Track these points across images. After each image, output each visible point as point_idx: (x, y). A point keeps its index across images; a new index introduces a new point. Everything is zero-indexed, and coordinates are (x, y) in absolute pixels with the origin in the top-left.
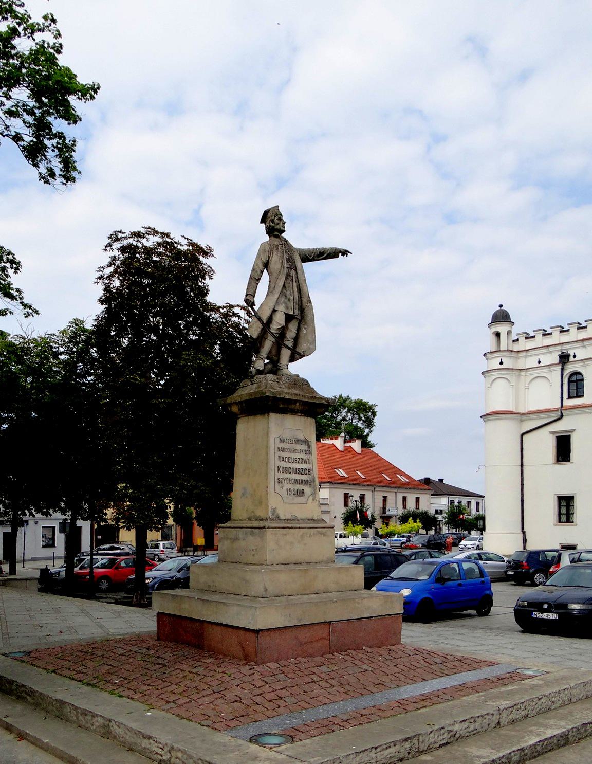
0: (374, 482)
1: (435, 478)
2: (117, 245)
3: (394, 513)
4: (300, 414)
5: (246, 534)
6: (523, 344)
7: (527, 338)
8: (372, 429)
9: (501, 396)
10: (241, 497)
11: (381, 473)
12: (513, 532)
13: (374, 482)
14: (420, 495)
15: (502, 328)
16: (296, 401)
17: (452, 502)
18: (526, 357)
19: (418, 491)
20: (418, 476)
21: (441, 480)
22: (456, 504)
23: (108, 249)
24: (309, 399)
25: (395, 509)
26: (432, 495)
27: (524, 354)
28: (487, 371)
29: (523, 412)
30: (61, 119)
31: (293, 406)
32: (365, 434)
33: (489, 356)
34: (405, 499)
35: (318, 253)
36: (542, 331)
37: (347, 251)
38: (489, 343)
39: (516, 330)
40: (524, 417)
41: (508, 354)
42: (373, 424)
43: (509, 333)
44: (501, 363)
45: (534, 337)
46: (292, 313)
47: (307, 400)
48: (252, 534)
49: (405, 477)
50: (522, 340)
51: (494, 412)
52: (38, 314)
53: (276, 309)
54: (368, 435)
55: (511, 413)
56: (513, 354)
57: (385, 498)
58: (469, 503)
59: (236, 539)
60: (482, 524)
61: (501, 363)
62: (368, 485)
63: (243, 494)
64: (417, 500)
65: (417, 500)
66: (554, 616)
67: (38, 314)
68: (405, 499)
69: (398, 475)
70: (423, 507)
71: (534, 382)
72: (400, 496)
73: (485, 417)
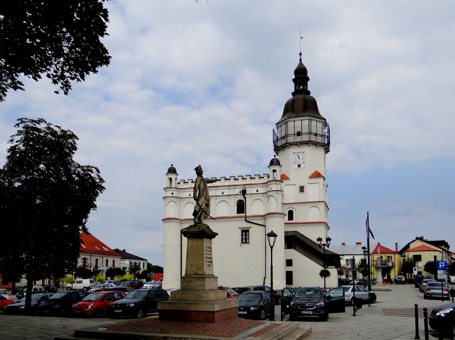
0: (91, 251)
1: (121, 249)
2: (22, 125)
3: (102, 269)
5: (195, 280)
6: (182, 186)
7: (184, 183)
8: (87, 220)
9: (172, 211)
10: (190, 267)
11: (94, 245)
12: (178, 279)
13: (91, 251)
14: (115, 258)
15: (173, 176)
17: (131, 263)
18: (184, 192)
19: (114, 257)
20: (113, 248)
21: (124, 251)
22: (133, 264)
23: (17, 126)
25: (103, 267)
26: (121, 259)
27: (183, 190)
28: (165, 197)
29: (182, 219)
32: (83, 222)
33: (166, 189)
34: (107, 261)
36: (191, 180)
38: (166, 184)
39: (179, 178)
40: (183, 222)
41: (175, 189)
42: (88, 217)
43: (176, 179)
44: (172, 194)
45: (188, 182)
48: (199, 280)
49: (107, 248)
50: (182, 183)
51: (169, 218)
54: (85, 223)
55: (177, 219)
56: (178, 190)
57: (97, 260)
58: (140, 263)
59: (191, 282)
60: (149, 275)
61: (172, 194)
62: (88, 253)
63: (191, 266)
64: (114, 261)
65: (114, 261)
66: (245, 313)
68: (107, 261)
69: (103, 247)
70: (117, 265)
71: (187, 205)
72: (105, 259)
73: (164, 220)
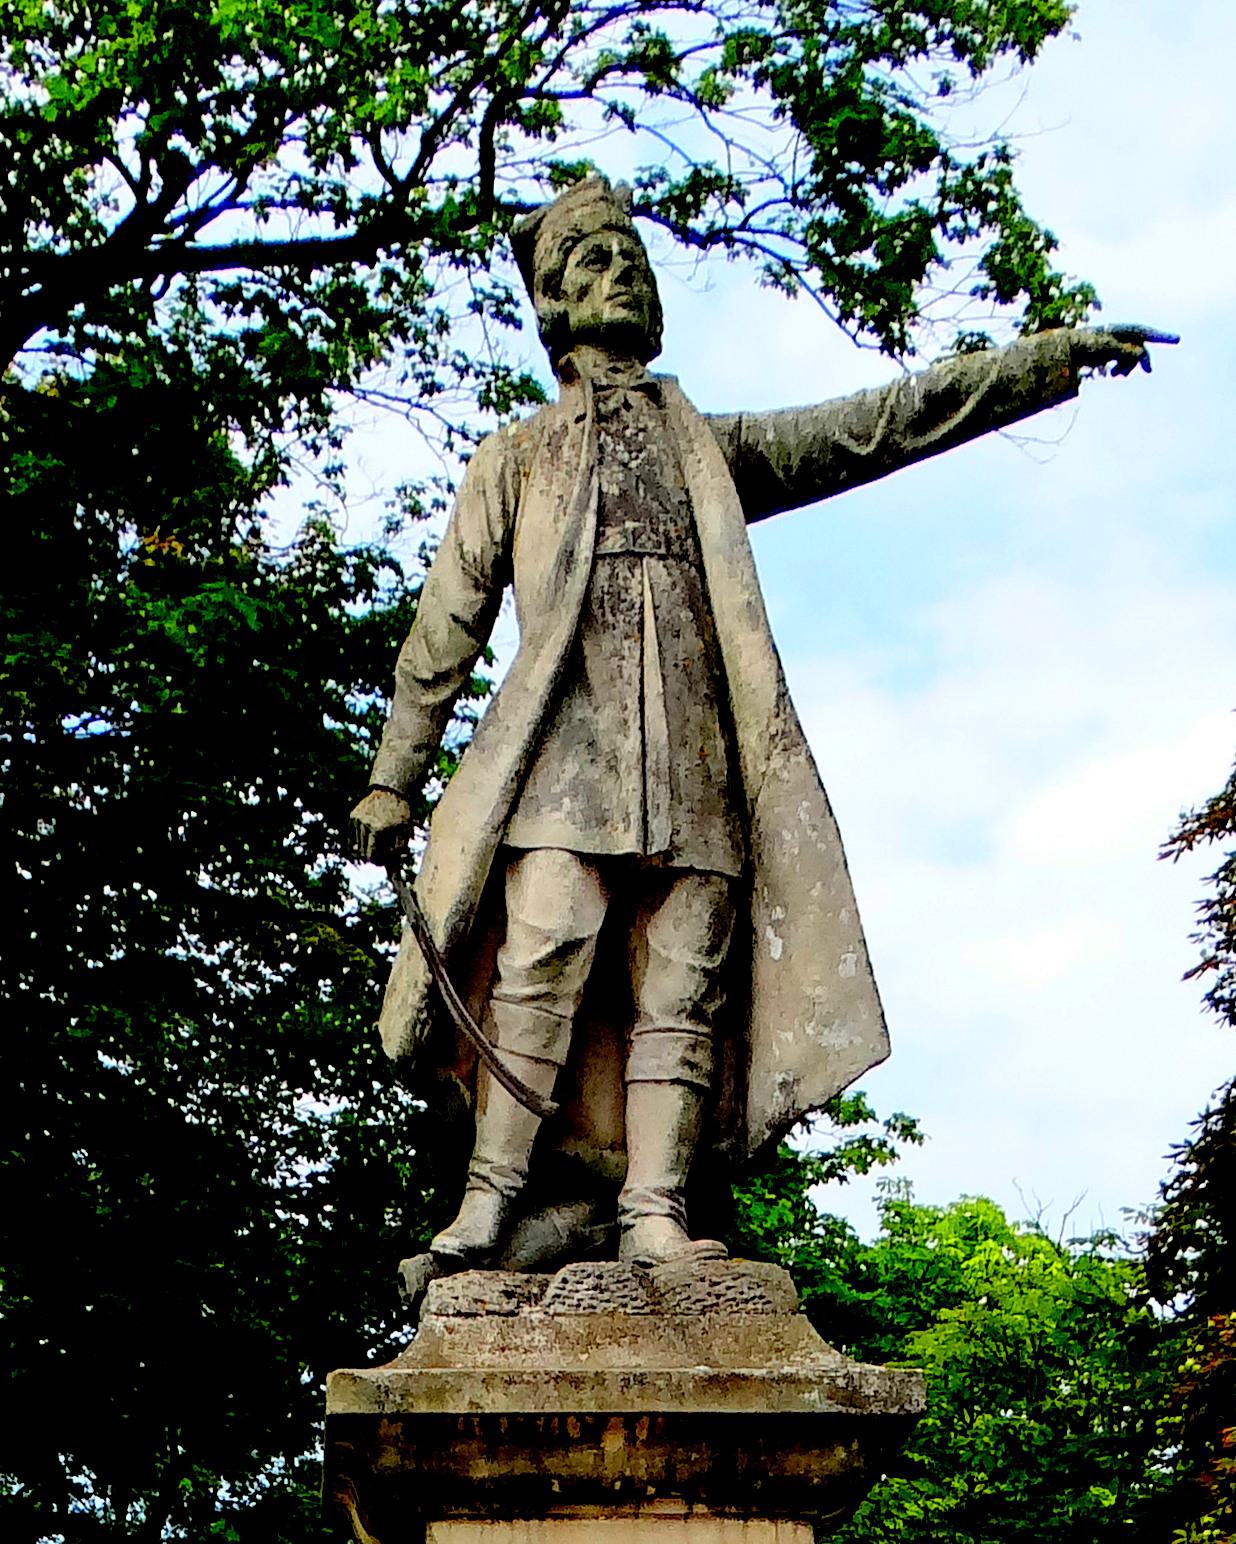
4: (680, 1508)
16: (594, 1427)
24: (680, 1397)
30: (872, 62)
31: (582, 1461)
35: (918, 404)
37: (1137, 336)
46: (626, 843)
47: (663, 1407)
52: (918, 1138)
53: (517, 840)
67: (918, 1138)
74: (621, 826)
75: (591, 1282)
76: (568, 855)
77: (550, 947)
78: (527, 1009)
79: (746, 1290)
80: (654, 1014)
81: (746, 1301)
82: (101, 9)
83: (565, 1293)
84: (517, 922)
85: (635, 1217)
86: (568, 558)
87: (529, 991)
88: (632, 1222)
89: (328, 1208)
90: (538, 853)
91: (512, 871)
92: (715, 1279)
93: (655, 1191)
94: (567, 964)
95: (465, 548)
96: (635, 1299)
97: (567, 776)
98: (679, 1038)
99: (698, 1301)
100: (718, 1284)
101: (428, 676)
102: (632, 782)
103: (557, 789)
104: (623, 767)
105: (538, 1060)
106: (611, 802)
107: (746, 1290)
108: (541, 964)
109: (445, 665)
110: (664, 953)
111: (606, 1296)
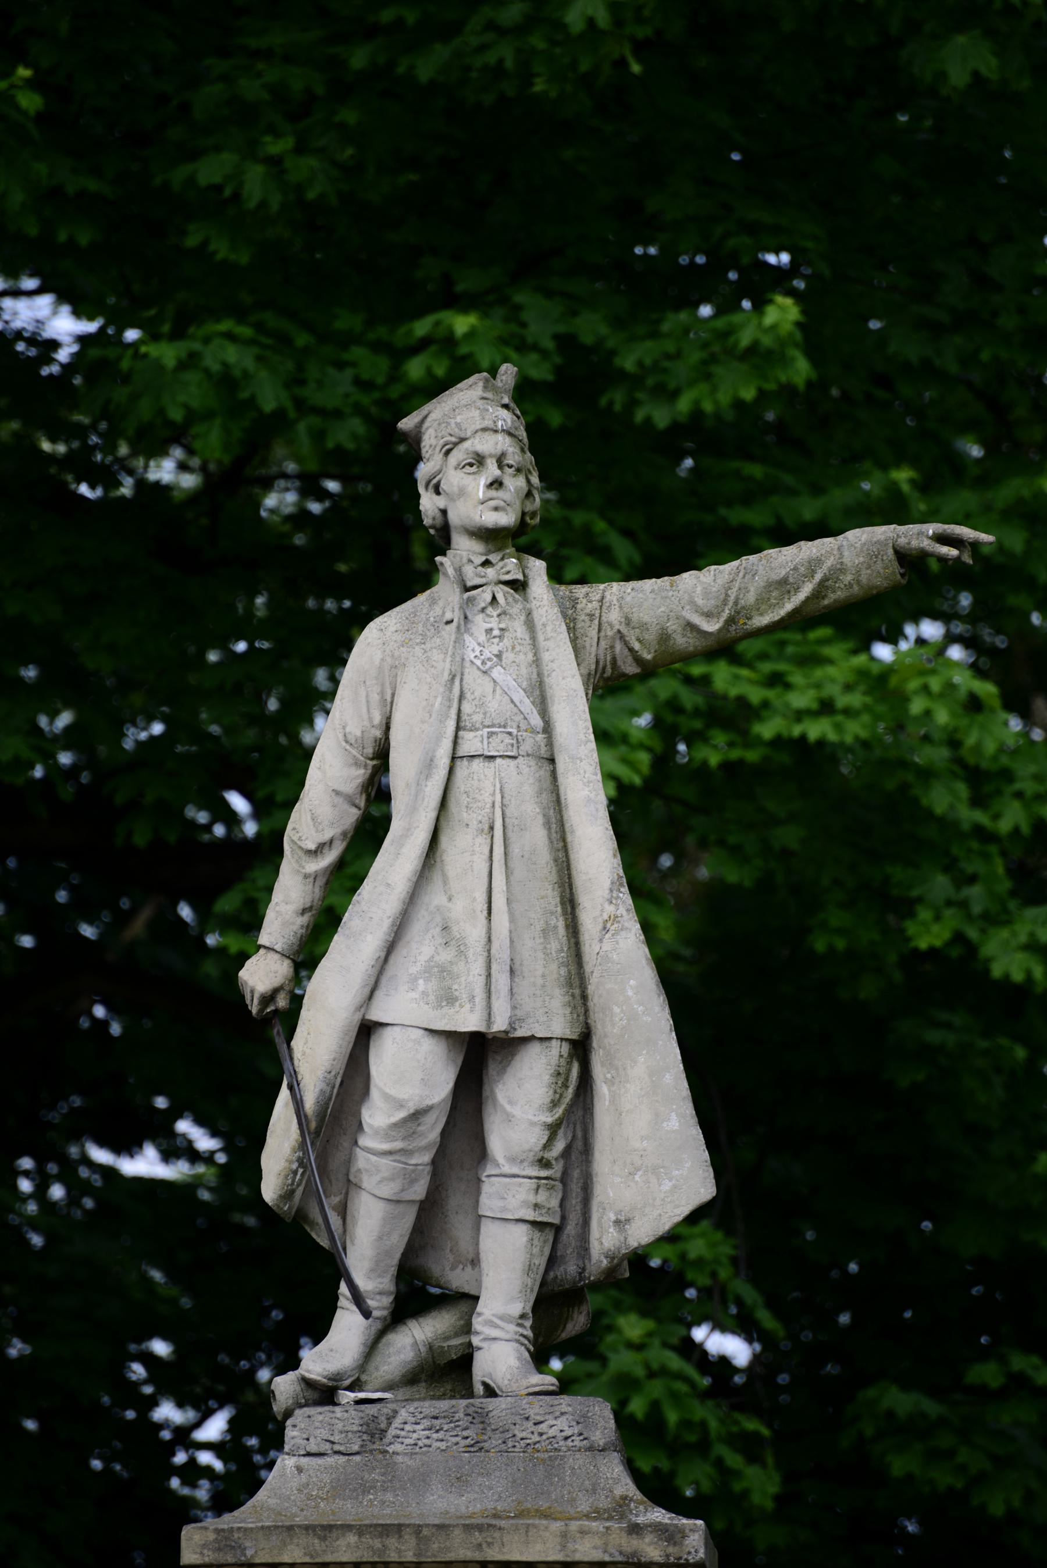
46: (470, 1021)
53: (376, 1014)
74: (468, 1006)
75: (426, 1423)
76: (422, 1032)
77: (402, 1114)
78: (385, 1161)
79: (566, 1428)
80: (501, 1160)
81: (566, 1438)
82: (322, 495)
83: (403, 1433)
84: (376, 1086)
85: (485, 1339)
86: (429, 764)
87: (385, 1146)
88: (480, 1344)
89: (160, 1348)
90: (395, 1028)
91: (174, 1160)
92: (539, 1418)
93: (501, 1318)
94: (419, 1125)
95: (348, 729)
96: (467, 1438)
97: (423, 958)
98: (520, 1184)
99: (522, 1439)
100: (542, 1422)
101: (312, 846)
102: (477, 967)
103: (414, 970)
104: (470, 954)
105: (398, 1202)
106: (459, 989)
107: (566, 1428)
108: (395, 1125)
109: (327, 836)
110: (508, 1107)
111: (440, 1435)
